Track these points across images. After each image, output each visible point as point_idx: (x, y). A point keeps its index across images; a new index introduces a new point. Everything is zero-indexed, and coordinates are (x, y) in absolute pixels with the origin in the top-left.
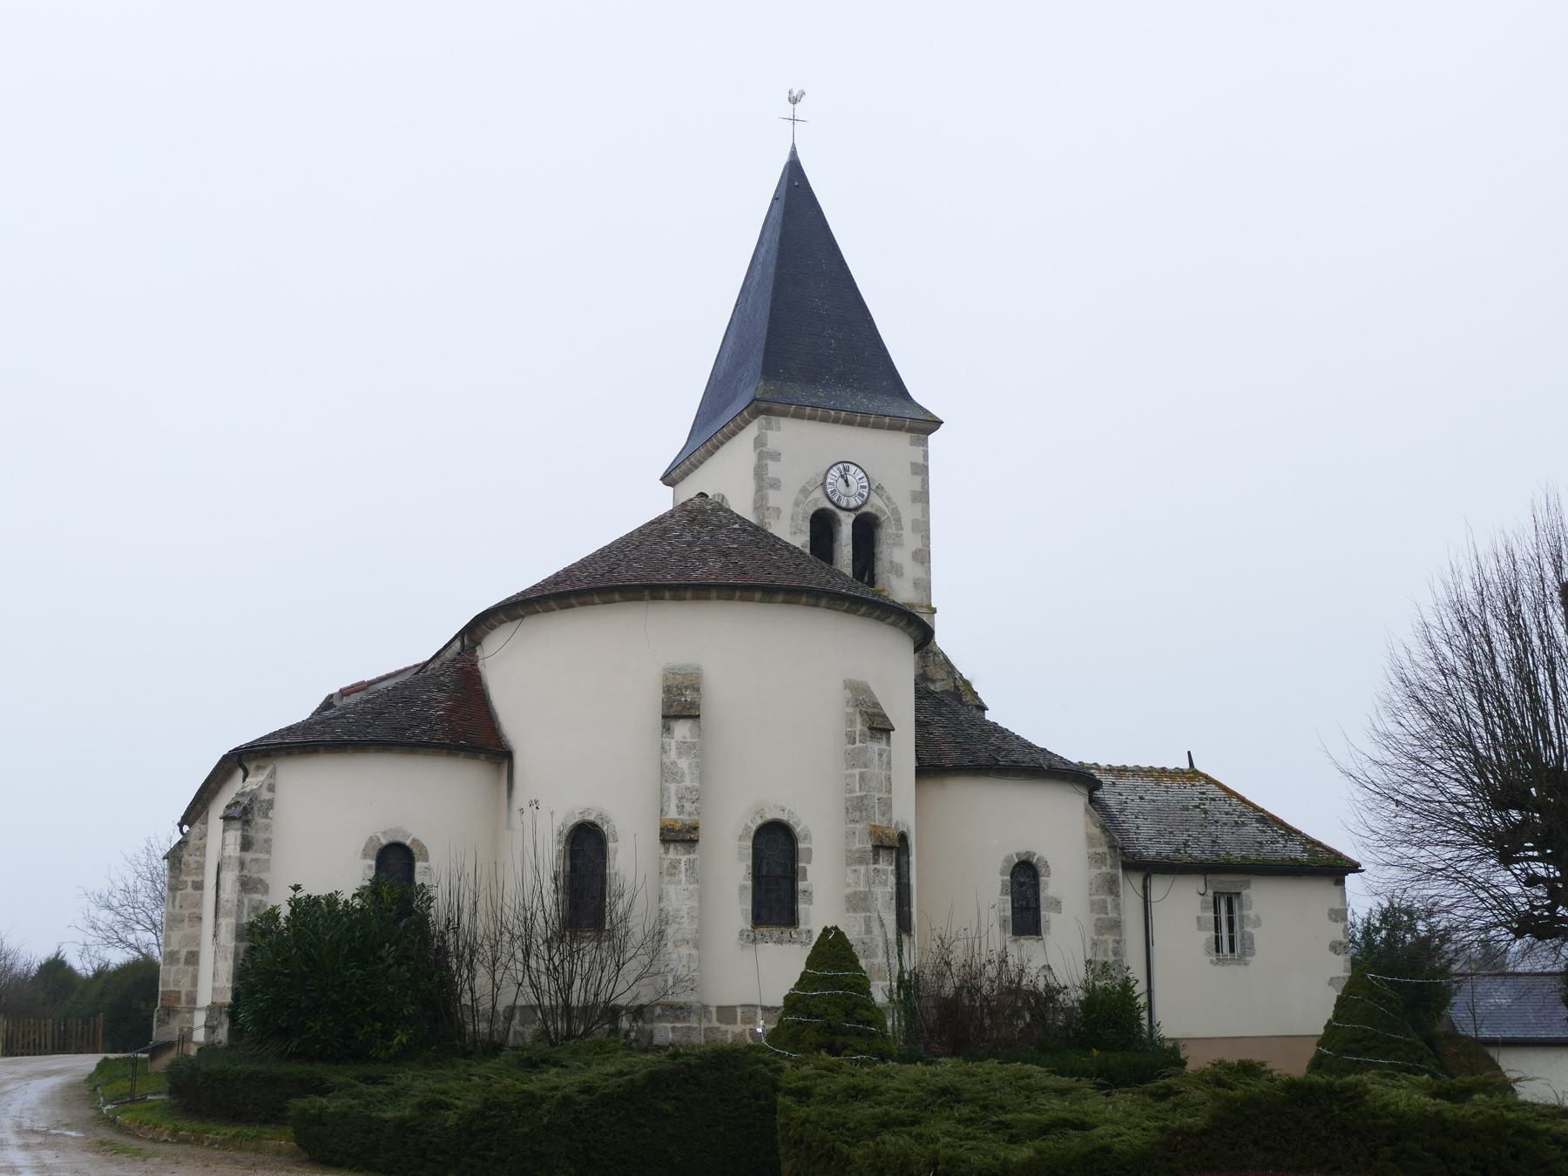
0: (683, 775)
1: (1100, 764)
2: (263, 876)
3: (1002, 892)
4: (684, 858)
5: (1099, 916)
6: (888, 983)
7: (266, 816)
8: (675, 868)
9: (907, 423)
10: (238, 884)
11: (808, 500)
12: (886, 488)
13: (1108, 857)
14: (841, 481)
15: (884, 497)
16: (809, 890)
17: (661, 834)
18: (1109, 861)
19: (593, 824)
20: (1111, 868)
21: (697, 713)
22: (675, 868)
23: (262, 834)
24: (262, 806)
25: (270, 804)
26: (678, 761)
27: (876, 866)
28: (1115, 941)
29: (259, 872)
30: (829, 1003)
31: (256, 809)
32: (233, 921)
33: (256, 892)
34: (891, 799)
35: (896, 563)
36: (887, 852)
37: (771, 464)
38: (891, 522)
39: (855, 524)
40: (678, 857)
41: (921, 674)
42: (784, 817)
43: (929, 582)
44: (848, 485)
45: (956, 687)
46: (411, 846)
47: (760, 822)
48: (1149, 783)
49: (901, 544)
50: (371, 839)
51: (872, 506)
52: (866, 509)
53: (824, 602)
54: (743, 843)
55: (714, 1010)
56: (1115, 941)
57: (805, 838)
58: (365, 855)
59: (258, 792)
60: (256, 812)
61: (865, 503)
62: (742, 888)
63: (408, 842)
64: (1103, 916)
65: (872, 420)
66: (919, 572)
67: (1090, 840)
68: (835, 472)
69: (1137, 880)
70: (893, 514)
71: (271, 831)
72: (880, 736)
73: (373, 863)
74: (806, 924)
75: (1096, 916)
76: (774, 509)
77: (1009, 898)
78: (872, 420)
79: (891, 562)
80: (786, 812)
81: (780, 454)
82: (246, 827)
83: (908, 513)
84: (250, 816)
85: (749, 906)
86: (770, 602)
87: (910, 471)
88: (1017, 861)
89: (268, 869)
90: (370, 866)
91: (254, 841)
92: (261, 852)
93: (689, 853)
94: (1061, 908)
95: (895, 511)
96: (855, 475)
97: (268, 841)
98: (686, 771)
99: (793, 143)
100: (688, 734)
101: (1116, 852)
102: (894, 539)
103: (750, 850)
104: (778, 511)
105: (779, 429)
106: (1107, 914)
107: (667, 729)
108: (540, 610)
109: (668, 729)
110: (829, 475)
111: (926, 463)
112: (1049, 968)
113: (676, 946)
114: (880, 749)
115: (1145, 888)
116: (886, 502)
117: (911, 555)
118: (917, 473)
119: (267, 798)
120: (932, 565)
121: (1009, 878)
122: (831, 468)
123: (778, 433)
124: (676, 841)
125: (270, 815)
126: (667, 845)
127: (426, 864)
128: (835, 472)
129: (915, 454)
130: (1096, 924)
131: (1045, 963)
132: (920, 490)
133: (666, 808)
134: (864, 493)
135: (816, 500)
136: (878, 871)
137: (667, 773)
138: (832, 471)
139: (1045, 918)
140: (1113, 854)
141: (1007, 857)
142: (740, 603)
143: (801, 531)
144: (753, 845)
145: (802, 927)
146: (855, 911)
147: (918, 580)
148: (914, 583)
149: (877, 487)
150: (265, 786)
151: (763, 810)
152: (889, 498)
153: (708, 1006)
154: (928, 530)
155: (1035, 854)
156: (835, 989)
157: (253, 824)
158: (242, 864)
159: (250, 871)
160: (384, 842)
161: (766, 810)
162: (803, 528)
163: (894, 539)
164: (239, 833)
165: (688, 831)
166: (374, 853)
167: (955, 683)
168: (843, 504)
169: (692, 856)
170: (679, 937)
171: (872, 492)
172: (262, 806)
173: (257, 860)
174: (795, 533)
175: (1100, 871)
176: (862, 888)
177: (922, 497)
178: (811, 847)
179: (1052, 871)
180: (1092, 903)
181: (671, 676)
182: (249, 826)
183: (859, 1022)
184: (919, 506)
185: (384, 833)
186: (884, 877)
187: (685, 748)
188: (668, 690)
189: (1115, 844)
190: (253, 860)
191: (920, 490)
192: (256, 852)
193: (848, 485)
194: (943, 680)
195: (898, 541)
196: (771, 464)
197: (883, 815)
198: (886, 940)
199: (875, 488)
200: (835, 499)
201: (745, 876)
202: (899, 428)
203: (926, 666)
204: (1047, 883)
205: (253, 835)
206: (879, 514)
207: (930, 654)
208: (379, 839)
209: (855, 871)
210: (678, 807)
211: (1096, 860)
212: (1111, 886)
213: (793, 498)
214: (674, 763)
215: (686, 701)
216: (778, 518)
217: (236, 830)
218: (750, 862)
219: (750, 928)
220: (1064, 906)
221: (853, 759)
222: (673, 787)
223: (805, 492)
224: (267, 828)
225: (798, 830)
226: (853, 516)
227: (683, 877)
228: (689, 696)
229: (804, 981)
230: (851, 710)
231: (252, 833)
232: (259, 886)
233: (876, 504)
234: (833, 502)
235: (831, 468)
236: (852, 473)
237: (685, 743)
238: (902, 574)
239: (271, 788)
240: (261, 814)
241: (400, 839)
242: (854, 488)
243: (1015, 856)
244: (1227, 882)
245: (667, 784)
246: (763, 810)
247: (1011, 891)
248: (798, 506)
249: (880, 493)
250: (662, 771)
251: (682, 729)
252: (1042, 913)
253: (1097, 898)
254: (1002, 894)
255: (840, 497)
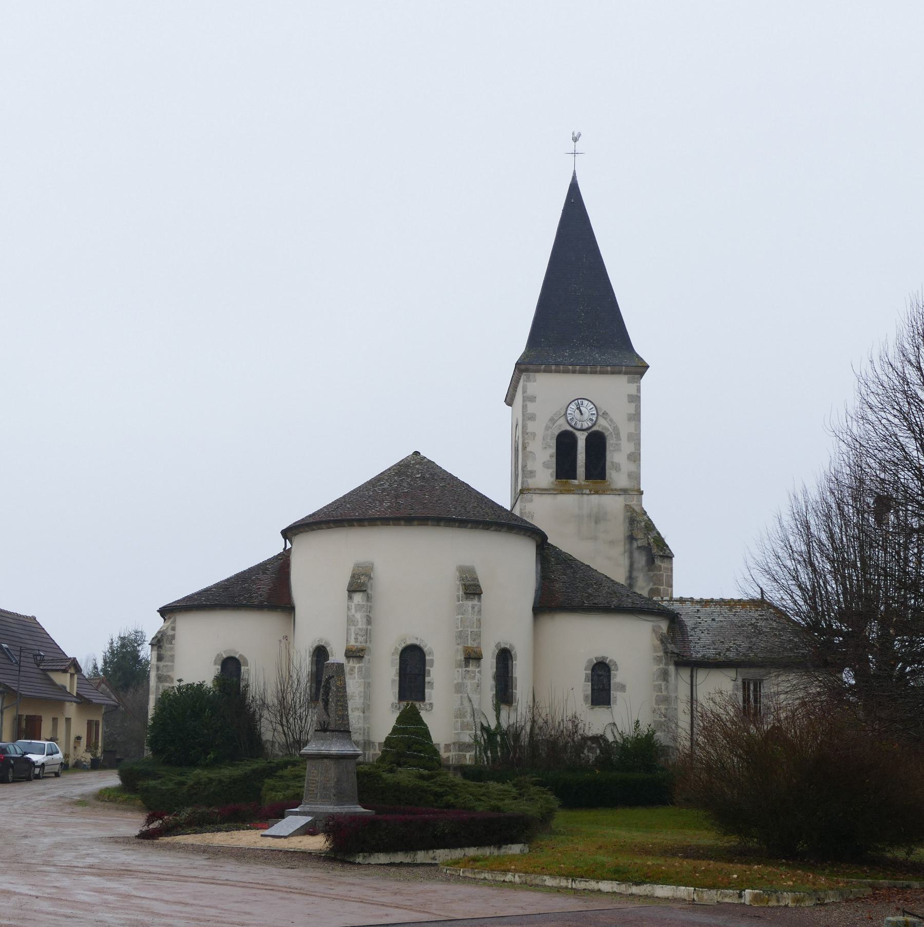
0: (358, 621)
1: (695, 598)
2: (169, 674)
3: (585, 680)
4: (357, 666)
5: (658, 694)
6: (474, 732)
7: (171, 643)
8: (352, 671)
9: (624, 369)
10: (156, 678)
11: (554, 426)
12: (609, 413)
13: (663, 658)
14: (577, 411)
15: (608, 420)
16: (432, 682)
17: (346, 653)
18: (664, 661)
19: (323, 647)
20: (665, 665)
21: (364, 589)
22: (352, 671)
23: (169, 653)
24: (168, 638)
25: (173, 637)
26: (356, 615)
27: (467, 669)
28: (665, 709)
29: (168, 672)
30: (400, 741)
31: (165, 640)
32: (154, 697)
33: (166, 682)
34: (480, 631)
35: (616, 463)
36: (474, 661)
37: (529, 405)
38: (612, 436)
39: (588, 440)
40: (354, 665)
41: (630, 535)
42: (417, 643)
43: (640, 474)
44: (582, 414)
45: (649, 544)
46: (239, 659)
47: (404, 645)
48: (725, 609)
49: (619, 450)
50: (218, 655)
51: (599, 426)
52: (595, 428)
53: (442, 523)
54: (394, 657)
55: (377, 745)
56: (665, 709)
57: (430, 653)
58: (215, 664)
59: (165, 631)
60: (165, 642)
61: (594, 425)
62: (393, 681)
63: (237, 656)
64: (660, 694)
65: (598, 369)
66: (632, 467)
67: (655, 649)
68: (573, 406)
69: (685, 674)
70: (614, 430)
71: (174, 651)
72: (473, 597)
73: (219, 667)
74: (429, 700)
75: (656, 694)
76: (531, 433)
77: (590, 684)
78: (598, 369)
79: (612, 462)
80: (419, 640)
81: (536, 397)
82: (160, 649)
83: (625, 429)
84: (161, 644)
85: (397, 690)
86: (411, 525)
87: (627, 400)
88: (595, 662)
89: (173, 670)
90: (218, 669)
91: (164, 656)
92: (168, 662)
93: (360, 663)
94: (625, 689)
95: (616, 429)
96: (587, 408)
97: (173, 656)
98: (359, 620)
99: (575, 170)
100: (360, 600)
101: (667, 655)
102: (614, 447)
103: (398, 661)
104: (534, 434)
105: (535, 381)
106: (662, 692)
107: (350, 598)
108: (316, 528)
109: (351, 597)
110: (569, 408)
111: (639, 394)
112: (614, 724)
113: (353, 711)
114: (473, 605)
115: (692, 677)
116: (610, 423)
117: (626, 457)
118: (632, 402)
119: (171, 634)
120: (641, 462)
121: (590, 672)
122: (570, 403)
123: (535, 384)
124: (353, 657)
125: (173, 642)
126: (349, 659)
127: (247, 668)
128: (573, 406)
129: (631, 389)
130: (656, 698)
131: (611, 721)
132: (634, 412)
133: (349, 640)
134: (593, 418)
135: (560, 426)
136: (468, 671)
137: (351, 621)
138: (571, 406)
139: (613, 695)
140: (666, 657)
141: (589, 660)
142: (394, 527)
143: (550, 446)
144: (400, 657)
145: (427, 701)
146: (457, 693)
147: (631, 473)
148: (629, 475)
149: (603, 413)
150: (170, 628)
151: (405, 639)
152: (611, 420)
153: (374, 743)
154: (639, 439)
155: (607, 658)
156: (404, 734)
157: (163, 647)
158: (158, 668)
159: (162, 671)
160: (225, 656)
161: (407, 639)
162: (551, 444)
163: (614, 447)
164: (156, 652)
165: (359, 652)
166: (220, 662)
167: (648, 541)
168: (579, 426)
169: (361, 665)
170: (354, 707)
171: (599, 417)
172: (168, 638)
173: (166, 666)
174: (546, 448)
175: (659, 667)
176: (460, 681)
177: (636, 417)
178: (433, 658)
179: (619, 668)
180: (655, 686)
181: (357, 568)
182: (162, 649)
183: (415, 751)
184: (633, 424)
185: (225, 652)
186: (472, 674)
187: (359, 608)
188: (353, 576)
189: (667, 650)
190: (164, 666)
191: (634, 412)
192: (166, 661)
193: (582, 414)
194: (642, 539)
195: (618, 449)
196: (529, 405)
197: (474, 640)
198: (473, 708)
199: (600, 413)
200: (573, 424)
201: (395, 675)
202: (619, 373)
203: (633, 530)
204: (615, 675)
205: (164, 653)
206: (604, 431)
207: (635, 522)
208: (222, 655)
209: (458, 671)
210: (355, 639)
211: (658, 660)
212: (665, 675)
213: (545, 425)
214: (353, 616)
215: (361, 582)
216: (534, 439)
217: (155, 651)
218: (398, 667)
219: (397, 702)
220: (627, 688)
221: (460, 610)
222: (353, 628)
223: (553, 420)
224: (172, 649)
225: (425, 649)
226: (586, 434)
227: (356, 675)
228: (363, 579)
229: (395, 730)
230: (458, 583)
231: (163, 652)
232: (168, 679)
233: (603, 425)
234: (572, 426)
235: (570, 403)
236: (585, 405)
237: (359, 605)
238: (620, 470)
239: (173, 629)
240: (168, 642)
241: (233, 655)
242: (586, 415)
243: (594, 659)
244: (752, 673)
245: (350, 627)
246: (405, 639)
247: (592, 680)
248: (548, 430)
249: (605, 416)
250: (348, 620)
251: (358, 598)
252: (612, 692)
253: (657, 683)
254: (585, 681)
255: (576, 422)
